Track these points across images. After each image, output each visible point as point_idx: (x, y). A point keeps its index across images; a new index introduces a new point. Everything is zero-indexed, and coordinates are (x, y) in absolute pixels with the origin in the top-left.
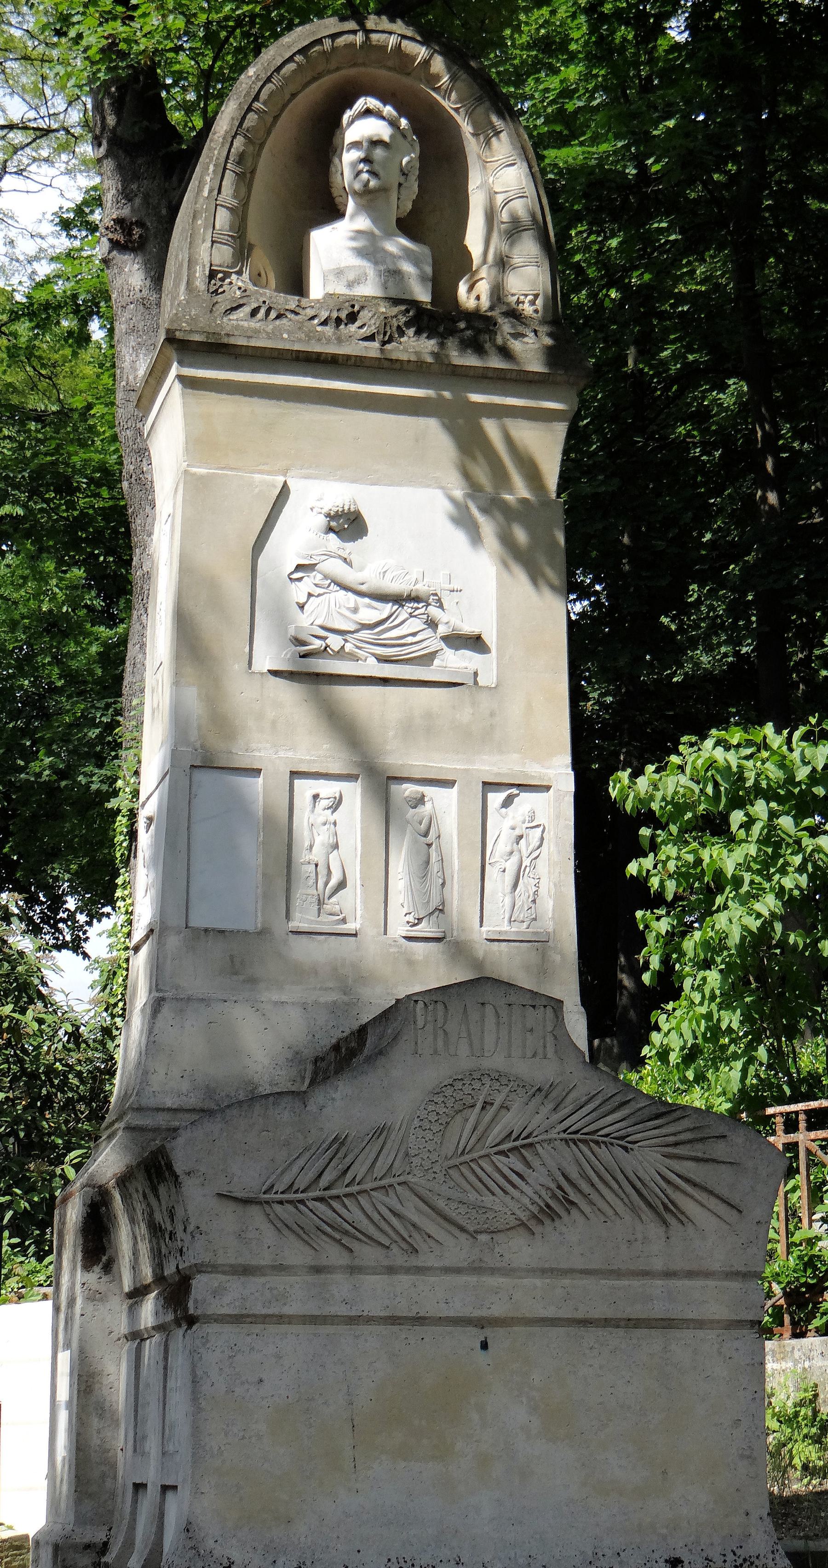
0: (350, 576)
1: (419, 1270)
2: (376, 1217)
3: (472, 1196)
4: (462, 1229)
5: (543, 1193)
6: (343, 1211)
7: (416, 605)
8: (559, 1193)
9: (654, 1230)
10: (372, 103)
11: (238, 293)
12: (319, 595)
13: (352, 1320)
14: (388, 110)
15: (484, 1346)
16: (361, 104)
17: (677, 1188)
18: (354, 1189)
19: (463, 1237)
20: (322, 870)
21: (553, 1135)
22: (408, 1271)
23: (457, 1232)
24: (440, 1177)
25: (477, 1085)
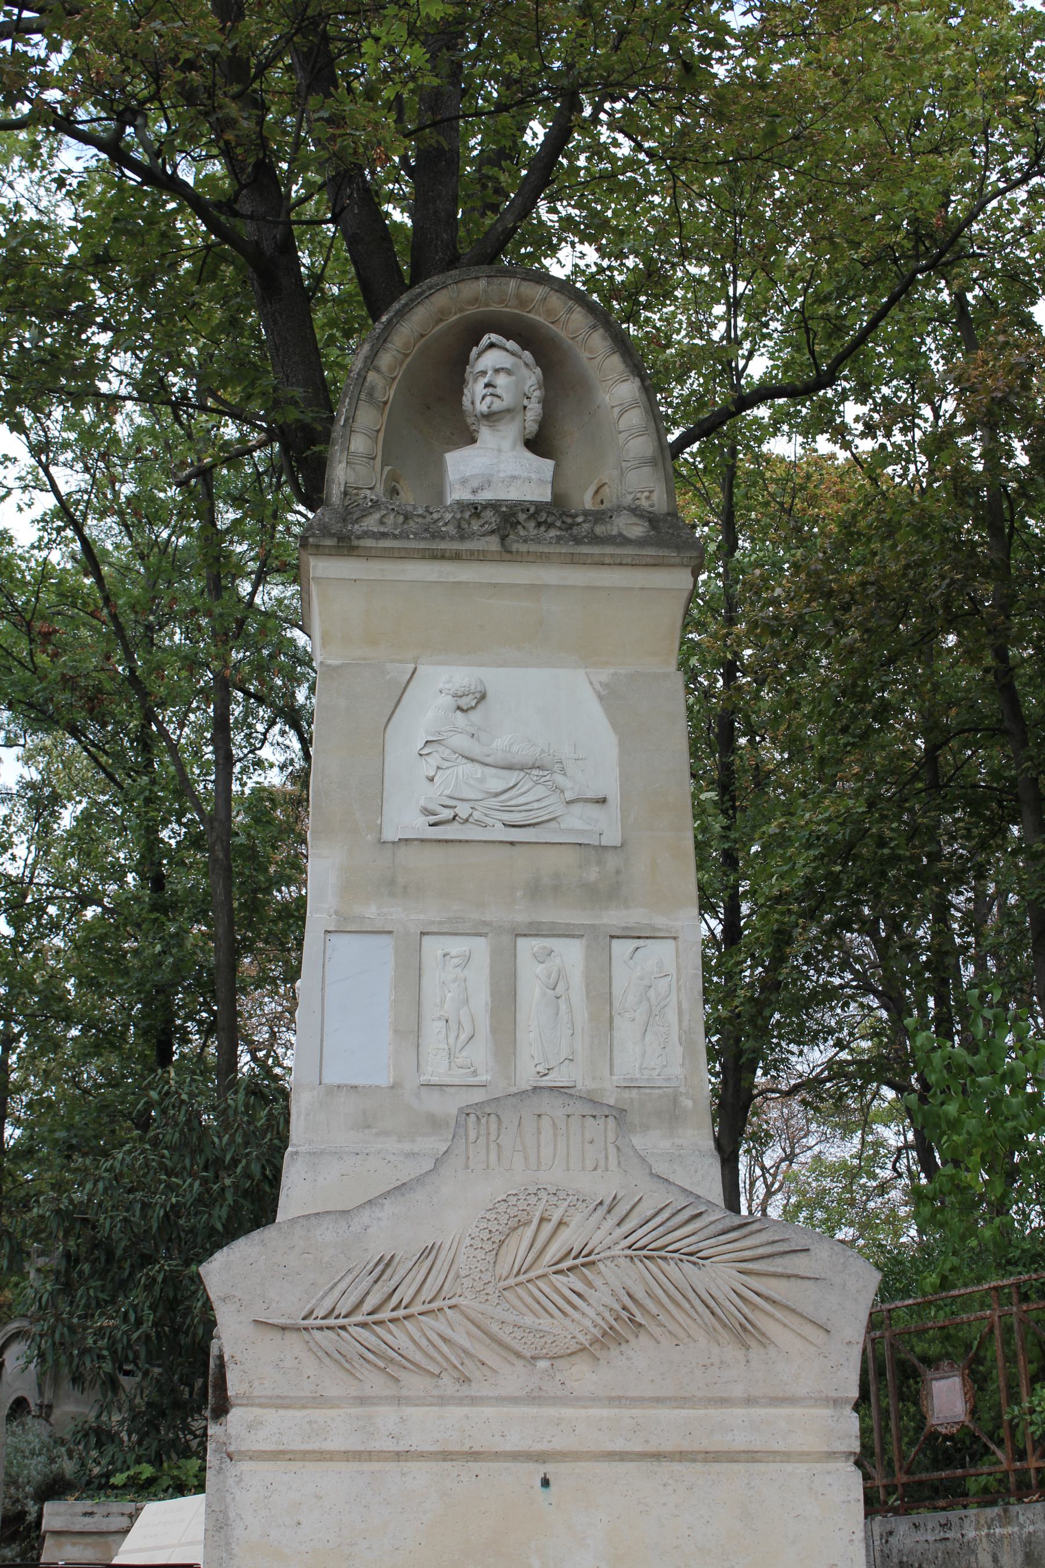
1: (474, 1401)
2: (424, 1343)
3: (529, 1320)
4: (519, 1355)
5: (607, 1314)
6: (388, 1338)
7: (541, 773)
8: (625, 1314)
9: (731, 1352)
10: (494, 337)
13: (398, 1456)
14: (511, 345)
15: (545, 1483)
16: (485, 341)
17: (755, 1307)
18: (401, 1313)
19: (519, 1363)
21: (616, 1251)
22: (460, 1401)
23: (513, 1358)
24: (494, 1299)
25: (533, 1200)
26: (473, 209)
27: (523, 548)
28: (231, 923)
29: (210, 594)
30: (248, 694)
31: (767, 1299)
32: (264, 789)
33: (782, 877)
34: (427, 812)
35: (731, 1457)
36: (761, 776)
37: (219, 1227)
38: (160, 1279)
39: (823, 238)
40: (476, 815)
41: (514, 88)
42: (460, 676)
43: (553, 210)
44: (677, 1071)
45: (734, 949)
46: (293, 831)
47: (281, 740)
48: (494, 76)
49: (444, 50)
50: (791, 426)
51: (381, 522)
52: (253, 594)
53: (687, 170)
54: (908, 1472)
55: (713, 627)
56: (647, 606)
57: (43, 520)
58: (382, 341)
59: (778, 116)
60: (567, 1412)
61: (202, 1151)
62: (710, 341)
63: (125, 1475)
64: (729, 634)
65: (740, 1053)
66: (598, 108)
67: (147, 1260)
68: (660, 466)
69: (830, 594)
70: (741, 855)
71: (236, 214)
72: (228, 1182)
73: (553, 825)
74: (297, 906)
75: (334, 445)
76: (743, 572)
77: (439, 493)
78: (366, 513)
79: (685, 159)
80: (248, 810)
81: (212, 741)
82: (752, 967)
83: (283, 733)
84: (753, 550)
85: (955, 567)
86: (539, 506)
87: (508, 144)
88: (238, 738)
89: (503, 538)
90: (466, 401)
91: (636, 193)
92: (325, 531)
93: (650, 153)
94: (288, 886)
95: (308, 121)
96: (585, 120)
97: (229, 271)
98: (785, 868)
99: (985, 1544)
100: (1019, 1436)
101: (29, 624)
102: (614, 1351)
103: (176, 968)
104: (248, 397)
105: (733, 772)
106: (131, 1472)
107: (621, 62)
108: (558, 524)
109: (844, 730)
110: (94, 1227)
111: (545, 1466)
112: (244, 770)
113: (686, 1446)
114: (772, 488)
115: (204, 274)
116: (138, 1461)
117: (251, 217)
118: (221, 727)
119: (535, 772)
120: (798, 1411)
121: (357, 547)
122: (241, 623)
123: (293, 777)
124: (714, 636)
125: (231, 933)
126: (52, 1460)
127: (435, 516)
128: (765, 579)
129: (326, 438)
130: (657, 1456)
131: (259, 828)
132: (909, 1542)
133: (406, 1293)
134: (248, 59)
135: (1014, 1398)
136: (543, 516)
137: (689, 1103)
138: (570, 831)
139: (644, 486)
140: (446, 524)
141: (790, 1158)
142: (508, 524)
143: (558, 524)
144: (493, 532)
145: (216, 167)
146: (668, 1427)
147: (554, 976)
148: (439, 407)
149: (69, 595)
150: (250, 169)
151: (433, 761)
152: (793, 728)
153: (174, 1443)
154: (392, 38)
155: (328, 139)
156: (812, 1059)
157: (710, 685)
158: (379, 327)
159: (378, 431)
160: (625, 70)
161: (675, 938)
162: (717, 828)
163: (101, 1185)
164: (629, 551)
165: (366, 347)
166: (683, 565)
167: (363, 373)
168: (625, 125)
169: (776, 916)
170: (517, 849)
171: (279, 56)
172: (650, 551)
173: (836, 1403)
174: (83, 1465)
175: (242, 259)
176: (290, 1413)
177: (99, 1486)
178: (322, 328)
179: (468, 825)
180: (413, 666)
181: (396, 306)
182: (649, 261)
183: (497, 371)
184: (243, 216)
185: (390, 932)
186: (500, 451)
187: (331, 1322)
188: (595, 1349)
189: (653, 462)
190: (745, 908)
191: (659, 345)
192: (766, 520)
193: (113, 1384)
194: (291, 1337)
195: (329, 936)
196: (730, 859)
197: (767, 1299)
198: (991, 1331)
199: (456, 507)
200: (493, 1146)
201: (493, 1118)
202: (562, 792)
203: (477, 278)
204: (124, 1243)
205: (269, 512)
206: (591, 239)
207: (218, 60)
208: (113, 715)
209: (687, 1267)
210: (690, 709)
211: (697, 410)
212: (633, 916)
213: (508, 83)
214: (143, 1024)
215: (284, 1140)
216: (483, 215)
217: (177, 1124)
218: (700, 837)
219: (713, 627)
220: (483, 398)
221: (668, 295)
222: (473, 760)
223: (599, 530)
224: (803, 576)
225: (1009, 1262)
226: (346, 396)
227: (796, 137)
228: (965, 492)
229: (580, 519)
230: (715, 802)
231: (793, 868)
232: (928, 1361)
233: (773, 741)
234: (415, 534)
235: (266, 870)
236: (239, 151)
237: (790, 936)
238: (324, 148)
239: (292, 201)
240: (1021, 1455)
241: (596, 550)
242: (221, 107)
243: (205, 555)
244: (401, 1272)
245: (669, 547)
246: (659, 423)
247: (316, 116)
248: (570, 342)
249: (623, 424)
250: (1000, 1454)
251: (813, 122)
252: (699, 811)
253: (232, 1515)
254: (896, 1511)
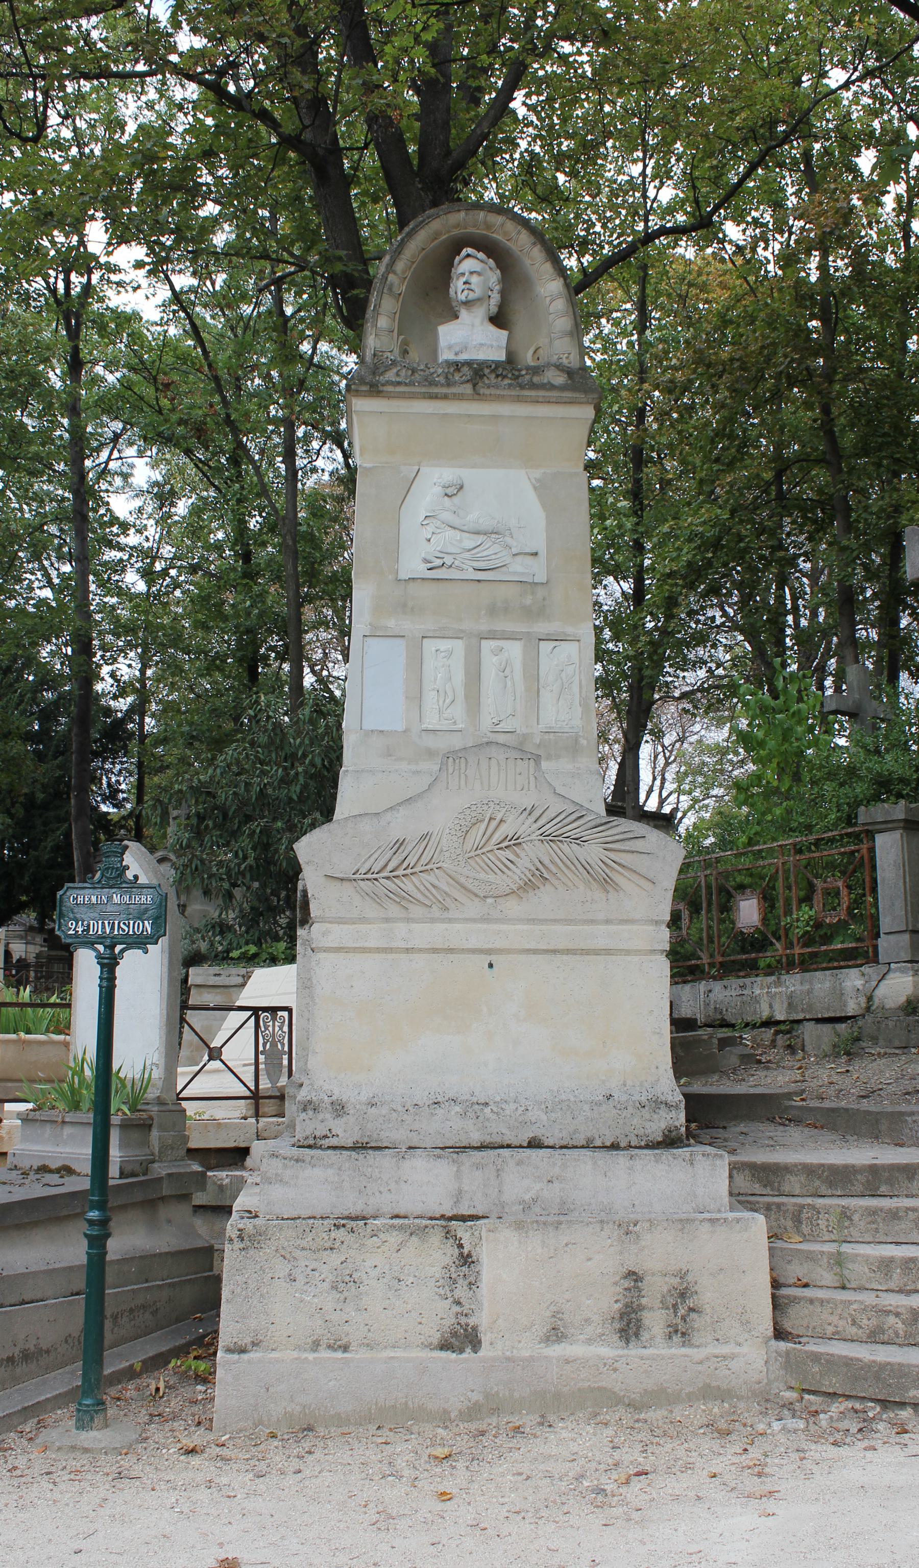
0: (457, 522)
1: (450, 920)
2: (422, 888)
3: (482, 875)
4: (476, 895)
5: (527, 873)
6: (402, 885)
8: (537, 873)
9: (599, 894)
10: (470, 250)
13: (408, 950)
14: (481, 255)
15: (491, 966)
16: (464, 252)
17: (613, 869)
18: (409, 871)
19: (477, 900)
20: (442, 693)
21: (533, 837)
22: (443, 921)
23: (473, 898)
24: (462, 864)
25: (485, 807)
27: (487, 392)
31: (619, 864)
33: (672, 560)
35: (596, 952)
37: (295, 798)
38: (258, 831)
44: (577, 722)
45: (638, 608)
47: (330, 455)
51: (398, 375)
54: (723, 956)
56: (563, 433)
57: (163, 305)
59: (667, 63)
60: (504, 927)
61: (282, 749)
63: (239, 952)
64: (640, 390)
65: (642, 678)
67: (249, 818)
69: (709, 366)
72: (300, 769)
73: (504, 569)
77: (434, 352)
78: (388, 369)
85: (795, 349)
86: (498, 364)
89: (474, 386)
90: (452, 291)
99: (765, 998)
100: (790, 935)
101: (155, 379)
102: (531, 893)
103: (260, 615)
106: (243, 950)
109: (717, 460)
110: (214, 797)
111: (490, 958)
113: (571, 946)
116: (247, 943)
120: (635, 927)
126: (193, 942)
127: (432, 370)
130: (554, 952)
132: (721, 997)
133: (412, 860)
135: (788, 912)
136: (500, 371)
137: (585, 742)
138: (515, 573)
141: (682, 740)
142: (477, 376)
146: (561, 935)
147: (504, 664)
148: (433, 294)
149: (184, 358)
151: (430, 529)
153: (268, 933)
156: (695, 677)
162: (629, 525)
163: (218, 771)
164: (555, 394)
166: (588, 403)
170: (481, 585)
172: (568, 394)
173: (657, 923)
174: (212, 945)
176: (346, 926)
177: (223, 958)
183: (472, 273)
186: (473, 325)
187: (369, 876)
188: (520, 893)
189: (571, 334)
193: (229, 896)
194: (346, 884)
197: (619, 864)
198: (777, 872)
200: (463, 776)
201: (463, 760)
204: (234, 808)
208: (213, 441)
209: (574, 846)
214: (239, 654)
215: (340, 758)
217: (266, 730)
223: (536, 379)
225: (791, 830)
228: (803, 297)
231: (679, 556)
232: (741, 887)
240: (790, 945)
241: (533, 393)
244: (410, 848)
249: (552, 309)
250: (778, 945)
253: (314, 981)
254: (714, 978)
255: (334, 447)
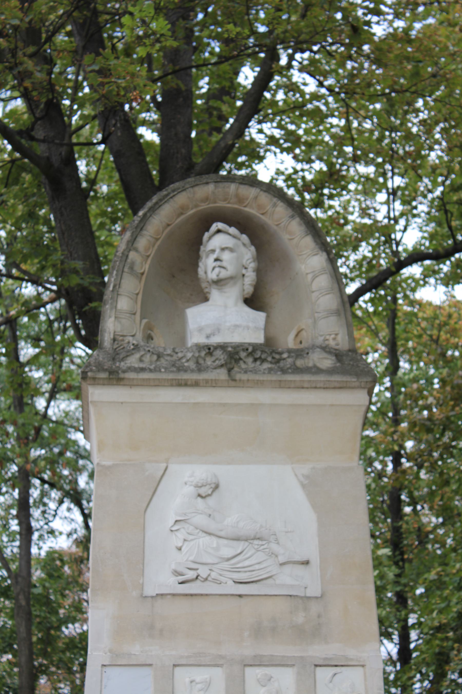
7: (261, 543)
10: (220, 225)
11: (132, 347)
12: (192, 540)
14: (233, 230)
26: (203, 131)
27: (244, 377)
28: (31, 653)
29: (15, 407)
30: (43, 481)
32: (55, 552)
33: (440, 612)
34: (177, 573)
36: (422, 535)
39: (456, 146)
40: (213, 575)
41: (232, 45)
42: (200, 472)
43: (260, 131)
45: (406, 667)
46: (77, 582)
47: (67, 514)
48: (218, 37)
49: (181, 20)
50: (436, 280)
51: (141, 360)
52: (47, 408)
53: (356, 101)
55: (383, 427)
56: (335, 420)
58: (140, 228)
59: (420, 61)
62: (376, 221)
64: (395, 432)
66: (291, 58)
68: (343, 315)
70: (409, 595)
71: (32, 139)
73: (269, 581)
74: (80, 639)
75: (105, 304)
76: (404, 386)
77: (183, 339)
78: (129, 354)
79: (355, 93)
80: (43, 568)
81: (17, 517)
82: (421, 681)
83: (69, 509)
84: (411, 370)
86: (255, 347)
87: (227, 84)
88: (36, 513)
89: (230, 370)
90: (201, 271)
91: (319, 117)
92: (100, 367)
93: (330, 89)
94: (73, 624)
95: (84, 71)
96: (282, 67)
97: (27, 177)
98: (443, 605)
104: (43, 268)
105: (401, 534)
107: (307, 26)
108: (269, 359)
112: (41, 537)
114: (424, 324)
115: (10, 181)
117: (44, 141)
118: (24, 506)
119: (256, 542)
121: (123, 379)
122: (38, 430)
123: (78, 542)
124: (385, 433)
125: (31, 660)
127: (180, 355)
128: (420, 391)
129: (100, 297)
131: (52, 581)
134: (40, 29)
136: (258, 354)
139: (330, 330)
140: (188, 361)
142: (232, 359)
143: (269, 359)
144: (222, 366)
145: (19, 103)
148: (181, 274)
150: (42, 106)
151: (181, 535)
152: (445, 500)
154: (143, 14)
155: (98, 85)
157: (383, 469)
158: (137, 219)
159: (137, 294)
160: (310, 32)
161: (363, 666)
164: (321, 378)
165: (128, 235)
166: (360, 387)
167: (126, 253)
168: (311, 69)
169: (437, 642)
170: (243, 600)
171: (63, 26)
175: (37, 170)
178: (96, 216)
179: (207, 583)
180: (164, 465)
181: (149, 204)
182: (331, 165)
183: (223, 249)
184: (37, 140)
185: (150, 665)
186: (226, 307)
189: (337, 313)
190: (413, 635)
191: (338, 224)
192: (420, 348)
195: (105, 669)
196: (401, 599)
199: (194, 348)
202: (277, 556)
203: (207, 183)
205: (58, 349)
206: (289, 150)
207: (19, 30)
210: (368, 487)
211: (368, 271)
212: (332, 650)
213: (226, 42)
216: (210, 134)
218: (379, 583)
219: (383, 427)
220: (214, 269)
221: (344, 188)
222: (210, 534)
223: (299, 363)
224: (448, 388)
226: (113, 268)
227: (434, 76)
229: (285, 355)
230: (389, 557)
231: (448, 606)
233: (431, 509)
234: (166, 368)
235: (57, 613)
236: (35, 93)
237: (448, 657)
238: (96, 91)
239: (73, 128)
241: (297, 378)
242: (21, 64)
243: (12, 382)
245: (350, 375)
246: (339, 280)
247: (90, 69)
248: (275, 227)
249: (315, 286)
251: (447, 64)
252: (378, 563)
255: (72, 506)
